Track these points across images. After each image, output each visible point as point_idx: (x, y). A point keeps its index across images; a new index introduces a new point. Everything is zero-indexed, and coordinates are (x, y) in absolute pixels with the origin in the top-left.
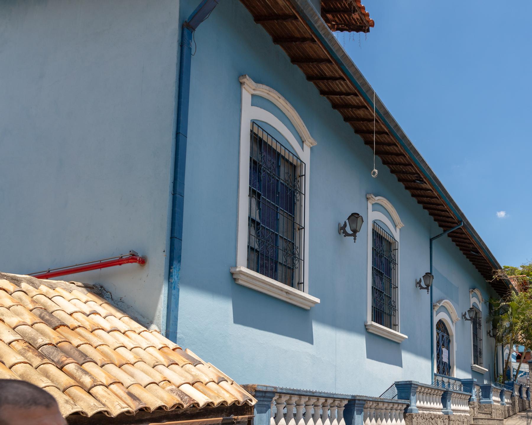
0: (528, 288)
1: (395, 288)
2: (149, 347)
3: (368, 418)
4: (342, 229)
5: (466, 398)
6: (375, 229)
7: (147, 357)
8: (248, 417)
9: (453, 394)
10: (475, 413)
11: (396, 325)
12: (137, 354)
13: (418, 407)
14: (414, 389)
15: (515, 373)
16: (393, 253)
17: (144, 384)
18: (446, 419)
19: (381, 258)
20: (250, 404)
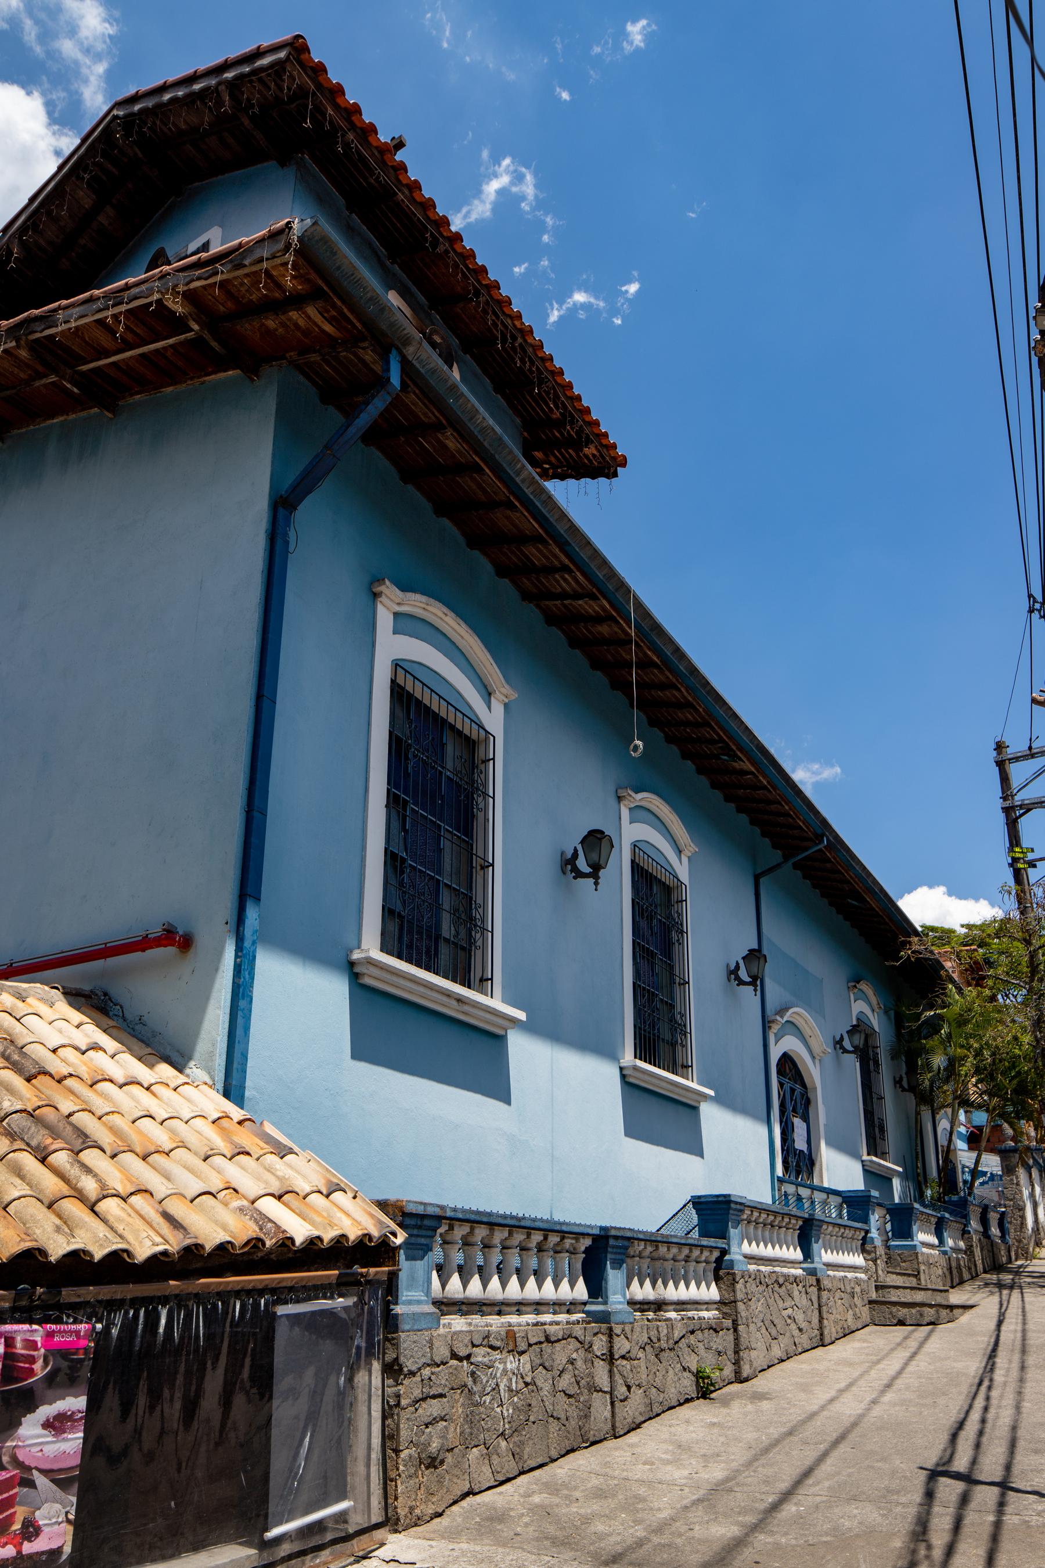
0: (983, 978)
1: (683, 984)
2: (196, 1117)
3: (648, 1279)
4: (568, 864)
5: (855, 1237)
6: (637, 861)
7: (192, 1140)
8: (389, 1271)
9: (825, 1227)
10: (880, 1272)
11: (687, 1067)
12: (173, 1132)
13: (746, 1256)
14: (736, 1213)
15: (968, 1177)
16: (676, 910)
17: (191, 1193)
18: (812, 1285)
19: (651, 920)
20: (393, 1242)
